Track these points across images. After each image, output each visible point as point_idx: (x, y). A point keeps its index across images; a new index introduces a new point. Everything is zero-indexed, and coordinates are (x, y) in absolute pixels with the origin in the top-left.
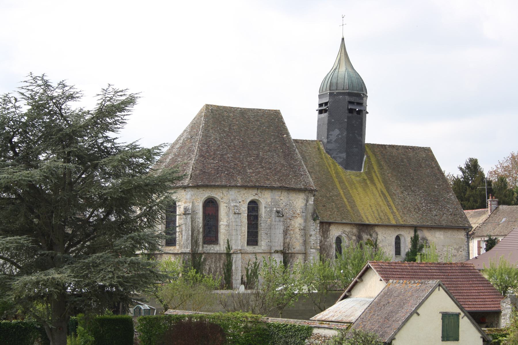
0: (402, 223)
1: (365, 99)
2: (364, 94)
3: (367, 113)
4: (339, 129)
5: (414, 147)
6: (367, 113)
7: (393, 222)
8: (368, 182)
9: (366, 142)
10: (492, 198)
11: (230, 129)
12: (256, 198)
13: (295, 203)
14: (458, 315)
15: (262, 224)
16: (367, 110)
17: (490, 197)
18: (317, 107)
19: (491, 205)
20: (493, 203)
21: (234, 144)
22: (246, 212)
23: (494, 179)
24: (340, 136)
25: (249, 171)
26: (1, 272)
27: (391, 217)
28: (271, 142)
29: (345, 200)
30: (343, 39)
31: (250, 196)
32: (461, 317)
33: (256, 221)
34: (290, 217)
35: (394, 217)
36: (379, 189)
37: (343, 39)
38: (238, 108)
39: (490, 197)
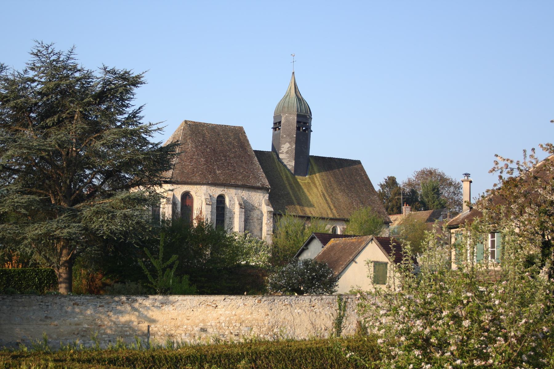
0: (338, 217)
1: (310, 120)
2: (309, 116)
3: (312, 131)
4: (290, 143)
5: (348, 160)
6: (312, 131)
7: (331, 216)
8: (312, 185)
9: (310, 154)
10: (406, 205)
11: (203, 139)
12: (222, 193)
13: (254, 198)
14: (386, 264)
15: (228, 214)
16: (312, 129)
17: (405, 205)
18: (272, 126)
19: (405, 210)
20: (407, 209)
21: (207, 151)
22: (216, 204)
23: (408, 190)
24: (290, 148)
25: (217, 172)
26: (2, 243)
27: (329, 212)
28: (235, 150)
29: (293, 198)
30: (293, 73)
31: (217, 191)
32: (388, 265)
33: (219, 207)
34: (250, 209)
35: (355, 348)
36: (320, 190)
37: (293, 73)
38: (210, 124)
39: (405, 205)
